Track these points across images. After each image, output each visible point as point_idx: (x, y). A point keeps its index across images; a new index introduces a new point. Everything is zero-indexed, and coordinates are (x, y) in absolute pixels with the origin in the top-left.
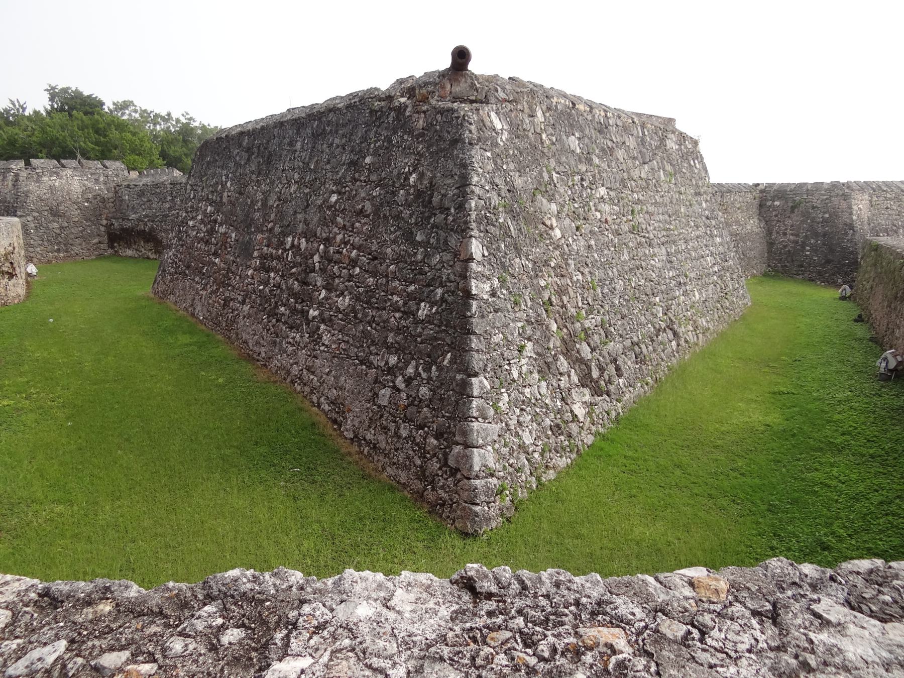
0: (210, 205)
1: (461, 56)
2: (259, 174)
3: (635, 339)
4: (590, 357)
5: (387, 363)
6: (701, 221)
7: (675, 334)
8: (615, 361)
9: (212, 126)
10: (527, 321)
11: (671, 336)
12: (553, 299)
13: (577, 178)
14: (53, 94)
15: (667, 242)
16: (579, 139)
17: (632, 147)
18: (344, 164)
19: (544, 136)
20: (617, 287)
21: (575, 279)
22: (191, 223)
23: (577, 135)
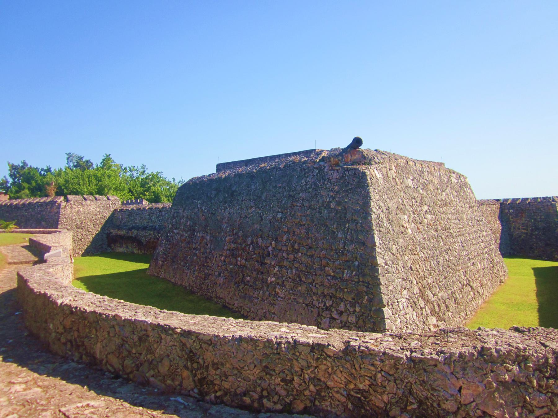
0: (190, 220)
1: (357, 142)
2: (226, 202)
3: (453, 290)
4: (433, 299)
5: (325, 305)
6: (475, 222)
7: (472, 287)
8: (445, 302)
9: (164, 176)
10: (403, 279)
11: (470, 289)
12: (413, 267)
13: (414, 201)
14: (69, 157)
15: (460, 235)
16: (412, 180)
17: (436, 183)
18: (285, 197)
19: (397, 179)
20: (440, 260)
21: (420, 256)
22: (176, 231)
23: (411, 178)
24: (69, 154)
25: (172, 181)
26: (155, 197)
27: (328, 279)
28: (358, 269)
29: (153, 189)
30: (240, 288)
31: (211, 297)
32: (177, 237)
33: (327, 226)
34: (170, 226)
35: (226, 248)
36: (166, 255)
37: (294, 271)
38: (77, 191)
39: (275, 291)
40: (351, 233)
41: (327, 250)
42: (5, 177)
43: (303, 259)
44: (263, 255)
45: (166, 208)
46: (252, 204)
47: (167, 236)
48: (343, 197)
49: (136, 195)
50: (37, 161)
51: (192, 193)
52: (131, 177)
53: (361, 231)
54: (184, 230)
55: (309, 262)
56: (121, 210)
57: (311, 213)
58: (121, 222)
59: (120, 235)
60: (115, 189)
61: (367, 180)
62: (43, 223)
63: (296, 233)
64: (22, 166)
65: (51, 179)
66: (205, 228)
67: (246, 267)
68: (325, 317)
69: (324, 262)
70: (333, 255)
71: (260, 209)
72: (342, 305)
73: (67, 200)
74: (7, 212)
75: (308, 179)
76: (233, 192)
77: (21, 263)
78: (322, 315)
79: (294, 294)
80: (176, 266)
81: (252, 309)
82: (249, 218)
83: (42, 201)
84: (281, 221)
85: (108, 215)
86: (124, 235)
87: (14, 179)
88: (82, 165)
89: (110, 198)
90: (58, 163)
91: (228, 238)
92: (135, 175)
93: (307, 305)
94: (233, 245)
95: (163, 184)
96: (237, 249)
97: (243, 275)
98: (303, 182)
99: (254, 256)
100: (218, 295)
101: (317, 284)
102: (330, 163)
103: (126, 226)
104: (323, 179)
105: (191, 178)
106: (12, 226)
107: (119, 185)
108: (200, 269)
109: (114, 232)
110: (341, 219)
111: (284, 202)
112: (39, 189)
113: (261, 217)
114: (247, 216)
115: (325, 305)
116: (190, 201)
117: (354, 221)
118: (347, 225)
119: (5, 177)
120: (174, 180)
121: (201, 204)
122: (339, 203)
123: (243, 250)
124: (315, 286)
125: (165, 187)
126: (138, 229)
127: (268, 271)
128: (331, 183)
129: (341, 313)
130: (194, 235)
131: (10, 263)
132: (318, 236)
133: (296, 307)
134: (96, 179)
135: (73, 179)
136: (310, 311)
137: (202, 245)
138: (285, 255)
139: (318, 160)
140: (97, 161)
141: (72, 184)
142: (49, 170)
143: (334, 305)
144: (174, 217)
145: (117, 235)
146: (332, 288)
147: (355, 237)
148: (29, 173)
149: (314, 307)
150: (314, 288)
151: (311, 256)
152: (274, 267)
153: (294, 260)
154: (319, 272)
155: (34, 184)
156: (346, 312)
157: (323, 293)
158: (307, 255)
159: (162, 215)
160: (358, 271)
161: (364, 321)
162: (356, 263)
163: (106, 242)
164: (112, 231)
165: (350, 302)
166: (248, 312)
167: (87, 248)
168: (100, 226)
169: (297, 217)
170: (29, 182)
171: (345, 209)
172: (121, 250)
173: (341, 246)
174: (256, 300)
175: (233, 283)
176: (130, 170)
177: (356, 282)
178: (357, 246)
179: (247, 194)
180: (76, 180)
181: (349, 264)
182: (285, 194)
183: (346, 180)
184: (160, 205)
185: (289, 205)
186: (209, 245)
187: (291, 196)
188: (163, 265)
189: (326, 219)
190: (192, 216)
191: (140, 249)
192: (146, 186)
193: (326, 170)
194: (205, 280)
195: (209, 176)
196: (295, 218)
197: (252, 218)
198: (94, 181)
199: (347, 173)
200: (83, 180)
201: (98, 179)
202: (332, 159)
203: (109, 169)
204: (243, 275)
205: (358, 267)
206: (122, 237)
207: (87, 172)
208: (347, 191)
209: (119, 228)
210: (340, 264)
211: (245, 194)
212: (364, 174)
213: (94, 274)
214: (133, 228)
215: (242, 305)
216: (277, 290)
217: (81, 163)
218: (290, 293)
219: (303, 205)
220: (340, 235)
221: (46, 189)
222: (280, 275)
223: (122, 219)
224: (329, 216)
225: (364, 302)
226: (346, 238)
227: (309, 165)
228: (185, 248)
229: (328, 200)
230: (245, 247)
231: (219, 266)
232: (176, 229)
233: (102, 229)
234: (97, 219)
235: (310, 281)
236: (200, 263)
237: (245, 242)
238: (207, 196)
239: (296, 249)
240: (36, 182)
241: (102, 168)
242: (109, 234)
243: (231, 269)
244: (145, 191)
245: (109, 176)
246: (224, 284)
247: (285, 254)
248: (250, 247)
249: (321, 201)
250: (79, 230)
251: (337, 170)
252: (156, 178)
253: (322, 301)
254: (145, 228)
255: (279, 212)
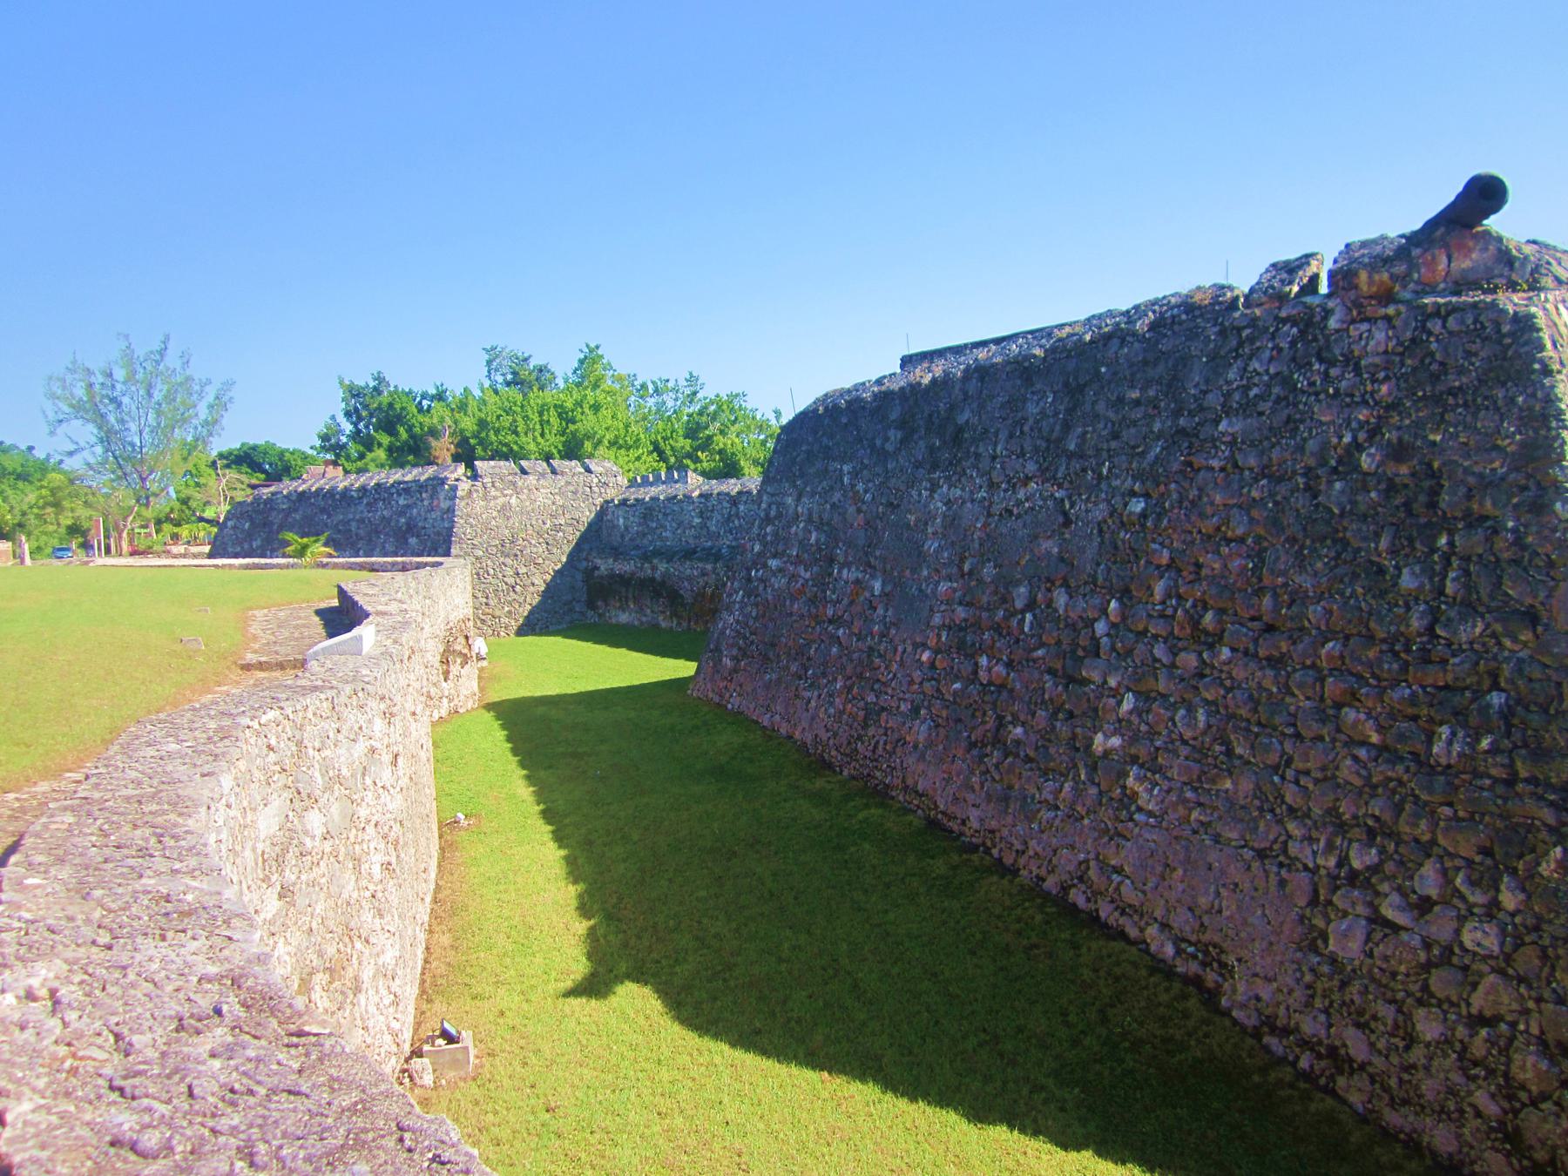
1: (1485, 194)
2: (935, 467)
5: (1343, 861)
22: (773, 563)
24: (493, 349)
25: (772, 417)
26: (726, 465)
27: (1355, 758)
28: (1509, 726)
29: (720, 442)
30: (990, 762)
31: (887, 786)
32: (779, 582)
33: (1345, 543)
34: (757, 548)
35: (937, 619)
36: (745, 638)
37: (1201, 716)
38: (511, 450)
39: (1124, 787)
40: (1467, 573)
41: (1347, 638)
42: (333, 418)
43: (1239, 673)
44: (1073, 652)
45: (749, 493)
46: (1031, 467)
47: (749, 580)
48: (1419, 424)
49: (672, 460)
50: (411, 376)
51: (825, 440)
52: (658, 410)
53: (1515, 562)
54: (798, 561)
55: (1267, 683)
56: (624, 502)
57: (1272, 495)
58: (622, 536)
59: (620, 576)
60: (613, 444)
61: (1542, 348)
62: (413, 541)
63: (1204, 572)
64: (375, 389)
65: (442, 420)
66: (866, 554)
67: (1012, 691)
68: (1345, 914)
69: (1332, 686)
70: (1380, 661)
71: (1060, 486)
72: (1429, 870)
73: (475, 477)
74: (323, 510)
75: (1255, 365)
76: (960, 430)
77: (281, 666)
78: (1329, 902)
79: (1200, 804)
80: (774, 676)
81: (1032, 843)
82: (1019, 516)
83: (409, 478)
84: (1143, 526)
85: (587, 515)
86: (633, 574)
87: (356, 425)
88: (527, 378)
89: (593, 467)
90: (465, 375)
91: (943, 587)
92: (670, 404)
93: (1261, 854)
94: (961, 613)
95: (749, 427)
96: (977, 626)
97: (1000, 718)
98: (1231, 376)
99: (1040, 652)
100: (910, 782)
101: (1307, 773)
102: (1352, 295)
103: (637, 547)
104: (1321, 360)
105: (820, 393)
106: (319, 548)
107: (622, 432)
108: (850, 689)
109: (605, 565)
110: (1410, 513)
111: (1151, 456)
112: (415, 450)
113: (1065, 514)
114: (1010, 512)
115: (1343, 861)
116: (819, 465)
117: (1475, 521)
118: (1443, 540)
119: (333, 418)
120: (778, 414)
121: (855, 474)
122: (1399, 452)
123: (997, 629)
124: (1297, 782)
125: (752, 437)
126: (668, 555)
127: (1096, 710)
128: (1357, 370)
129: (1424, 906)
130: (830, 575)
131: (247, 667)
132: (1305, 581)
133: (1213, 857)
134: (560, 415)
135: (498, 417)
136: (1273, 879)
137: (856, 609)
138: (1159, 651)
139: (1296, 289)
140: (563, 367)
141: (497, 432)
142: (440, 397)
143: (1389, 867)
144: (768, 520)
145: (612, 576)
146: (1373, 796)
147: (1484, 590)
148: (391, 405)
149: (1290, 864)
150: (1293, 787)
151: (1276, 662)
152: (1117, 694)
153: (1202, 676)
154: (1310, 728)
155: (403, 433)
156: (1446, 903)
157: (1332, 811)
158: (1256, 655)
159: (737, 515)
160: (1508, 735)
161: (1544, 956)
162: (1496, 699)
163: (586, 596)
164: (598, 561)
165: (1470, 863)
166: (1020, 853)
167: (531, 613)
168: (567, 549)
169: (1209, 510)
170: (392, 432)
171: (1433, 475)
172: (624, 618)
173: (1416, 623)
174: (1051, 814)
175: (964, 744)
176: (656, 390)
177: (1496, 780)
178: (1498, 628)
179: (1011, 436)
180: (506, 421)
181: (1457, 700)
182: (1157, 427)
183: (1432, 354)
184: (732, 486)
185: (1175, 467)
186: (880, 611)
187: (1182, 432)
188: (735, 670)
189: (1342, 514)
190: (826, 516)
191: (675, 614)
192: (698, 435)
193: (1333, 323)
194: (865, 726)
195: (879, 382)
196: (1202, 516)
197: (1028, 518)
198: (554, 420)
199: (1435, 326)
200: (526, 418)
201: (566, 417)
202: (1363, 276)
203: (596, 386)
204: (1000, 718)
205: (1507, 714)
206: (624, 581)
207: (536, 398)
208: (1437, 399)
209: (617, 553)
210: (1413, 700)
211: (1002, 436)
212: (1524, 324)
213: (538, 694)
214: (658, 553)
215: (994, 824)
216: (1130, 782)
217: (524, 374)
218: (1185, 801)
219: (1236, 465)
220: (1407, 581)
221: (428, 448)
222: (1143, 728)
223: (626, 528)
224: (1353, 503)
225: (1544, 869)
226: (1441, 592)
227: (1257, 312)
228: (802, 616)
229: (1347, 439)
230: (1006, 618)
231: (911, 682)
232: (774, 556)
233: (570, 556)
234: (557, 528)
235: (1273, 758)
236: (849, 670)
237: (1004, 600)
238: (873, 447)
239: (1207, 633)
240: (410, 429)
241: (578, 385)
242: (590, 572)
243: (955, 693)
244: (696, 449)
245: (596, 408)
246: (930, 744)
247: (1159, 651)
248: (1023, 620)
249: (1312, 445)
250: (509, 561)
251: (1388, 318)
252: (728, 410)
253: (1330, 846)
254: (689, 554)
255: (1133, 494)
